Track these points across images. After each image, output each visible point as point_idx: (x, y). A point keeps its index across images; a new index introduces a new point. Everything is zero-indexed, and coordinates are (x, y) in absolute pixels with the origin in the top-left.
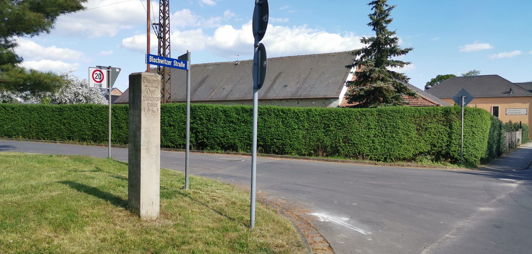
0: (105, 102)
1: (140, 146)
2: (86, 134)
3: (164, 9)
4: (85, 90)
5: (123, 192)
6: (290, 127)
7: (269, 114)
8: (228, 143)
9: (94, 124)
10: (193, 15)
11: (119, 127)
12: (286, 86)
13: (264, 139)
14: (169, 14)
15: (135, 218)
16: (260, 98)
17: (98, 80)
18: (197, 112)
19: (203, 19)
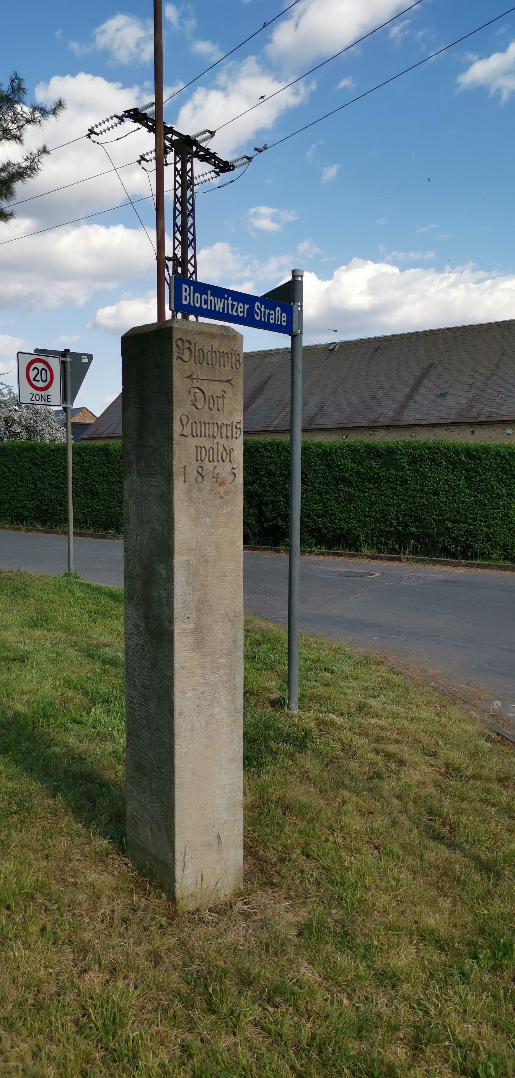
0: (62, 436)
1: (171, 620)
2: (24, 507)
3: (184, 222)
4: (26, 414)
5: (102, 739)
6: (487, 491)
7: (434, 460)
8: (335, 530)
9: (41, 486)
10: (235, 253)
11: (91, 491)
12: (444, 395)
13: (420, 521)
14: (194, 235)
15: (158, 902)
16: (248, 430)
17: (41, 384)
18: (262, 457)
19: (256, 262)
